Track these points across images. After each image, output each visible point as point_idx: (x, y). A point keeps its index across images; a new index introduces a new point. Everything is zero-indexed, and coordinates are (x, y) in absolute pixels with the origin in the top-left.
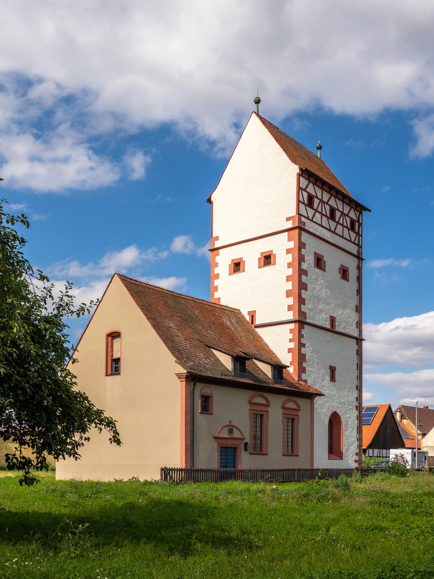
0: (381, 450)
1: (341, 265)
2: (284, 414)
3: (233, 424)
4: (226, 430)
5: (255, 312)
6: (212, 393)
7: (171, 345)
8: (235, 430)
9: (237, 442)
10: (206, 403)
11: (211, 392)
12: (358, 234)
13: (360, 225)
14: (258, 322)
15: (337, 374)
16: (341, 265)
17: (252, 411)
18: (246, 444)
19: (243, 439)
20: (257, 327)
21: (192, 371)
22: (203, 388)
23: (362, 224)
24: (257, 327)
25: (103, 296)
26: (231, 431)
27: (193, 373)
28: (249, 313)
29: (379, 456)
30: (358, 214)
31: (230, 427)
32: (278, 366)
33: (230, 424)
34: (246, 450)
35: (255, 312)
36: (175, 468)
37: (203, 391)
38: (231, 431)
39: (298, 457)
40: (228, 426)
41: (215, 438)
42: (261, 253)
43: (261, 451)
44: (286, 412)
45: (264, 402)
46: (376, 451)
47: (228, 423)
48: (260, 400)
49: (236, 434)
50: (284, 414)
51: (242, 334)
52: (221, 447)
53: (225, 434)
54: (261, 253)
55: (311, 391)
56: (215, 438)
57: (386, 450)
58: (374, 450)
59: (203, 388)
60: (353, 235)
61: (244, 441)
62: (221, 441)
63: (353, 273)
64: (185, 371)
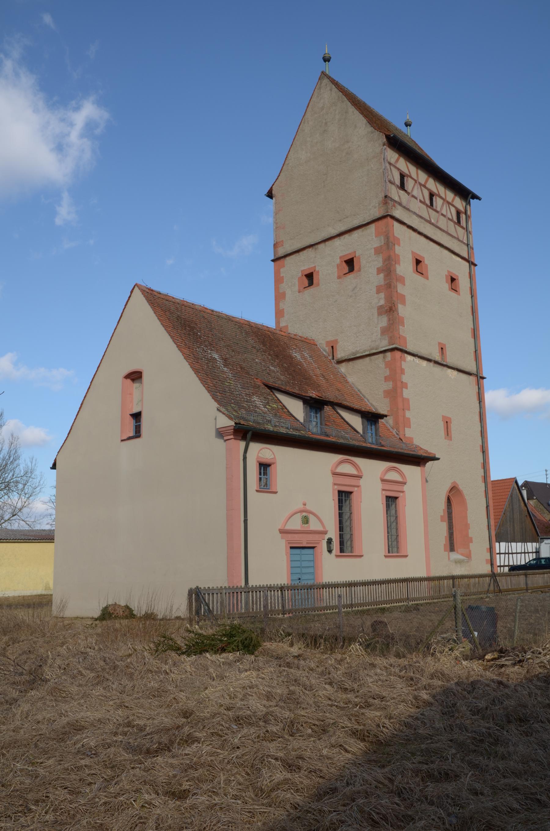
0: (525, 544)
1: (448, 272)
2: (383, 490)
3: (308, 507)
4: (298, 518)
5: (336, 341)
6: (275, 458)
7: (211, 385)
8: (312, 518)
9: (316, 537)
10: (343, 532)
11: (272, 456)
12: (466, 229)
13: (468, 218)
14: (340, 355)
15: (453, 427)
16: (448, 272)
17: (336, 487)
18: (330, 541)
19: (325, 533)
20: (340, 362)
21: (242, 422)
22: (261, 450)
23: (469, 217)
24: (340, 362)
25: (119, 320)
26: (306, 521)
27: (244, 425)
28: (328, 343)
29: (507, 552)
30: (464, 204)
31: (304, 514)
32: (370, 415)
33: (303, 509)
34: (330, 551)
35: (336, 341)
36: (209, 588)
37: (260, 455)
38: (306, 521)
39: (362, 558)
40: (301, 511)
41: (283, 532)
42: (340, 258)
43: (351, 552)
44: (388, 487)
45: (354, 472)
46: (503, 544)
47: (301, 506)
48: (347, 469)
49: (314, 525)
50: (383, 490)
51: (318, 372)
52: (291, 548)
53: (296, 524)
54: (340, 258)
55: (420, 453)
56: (283, 532)
57: (515, 543)
58: (517, 543)
59: (261, 450)
60: (461, 233)
61: (327, 537)
62: (290, 536)
63: (464, 283)
64: (232, 423)
